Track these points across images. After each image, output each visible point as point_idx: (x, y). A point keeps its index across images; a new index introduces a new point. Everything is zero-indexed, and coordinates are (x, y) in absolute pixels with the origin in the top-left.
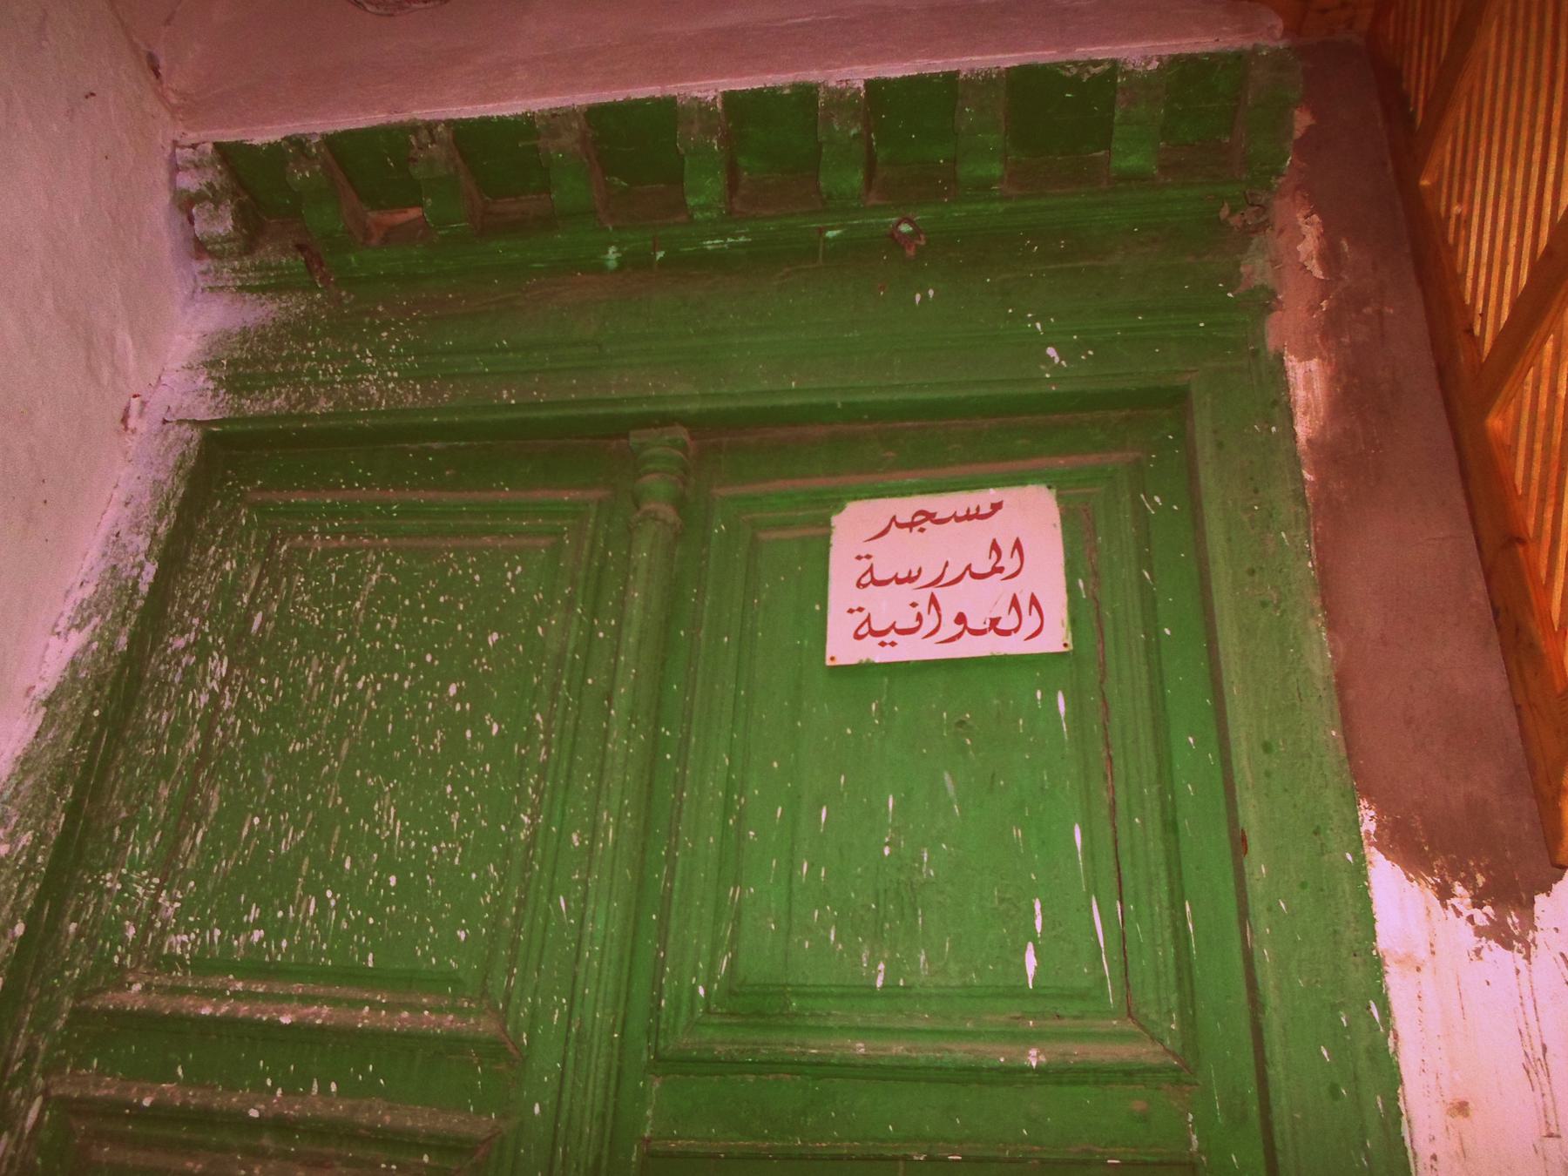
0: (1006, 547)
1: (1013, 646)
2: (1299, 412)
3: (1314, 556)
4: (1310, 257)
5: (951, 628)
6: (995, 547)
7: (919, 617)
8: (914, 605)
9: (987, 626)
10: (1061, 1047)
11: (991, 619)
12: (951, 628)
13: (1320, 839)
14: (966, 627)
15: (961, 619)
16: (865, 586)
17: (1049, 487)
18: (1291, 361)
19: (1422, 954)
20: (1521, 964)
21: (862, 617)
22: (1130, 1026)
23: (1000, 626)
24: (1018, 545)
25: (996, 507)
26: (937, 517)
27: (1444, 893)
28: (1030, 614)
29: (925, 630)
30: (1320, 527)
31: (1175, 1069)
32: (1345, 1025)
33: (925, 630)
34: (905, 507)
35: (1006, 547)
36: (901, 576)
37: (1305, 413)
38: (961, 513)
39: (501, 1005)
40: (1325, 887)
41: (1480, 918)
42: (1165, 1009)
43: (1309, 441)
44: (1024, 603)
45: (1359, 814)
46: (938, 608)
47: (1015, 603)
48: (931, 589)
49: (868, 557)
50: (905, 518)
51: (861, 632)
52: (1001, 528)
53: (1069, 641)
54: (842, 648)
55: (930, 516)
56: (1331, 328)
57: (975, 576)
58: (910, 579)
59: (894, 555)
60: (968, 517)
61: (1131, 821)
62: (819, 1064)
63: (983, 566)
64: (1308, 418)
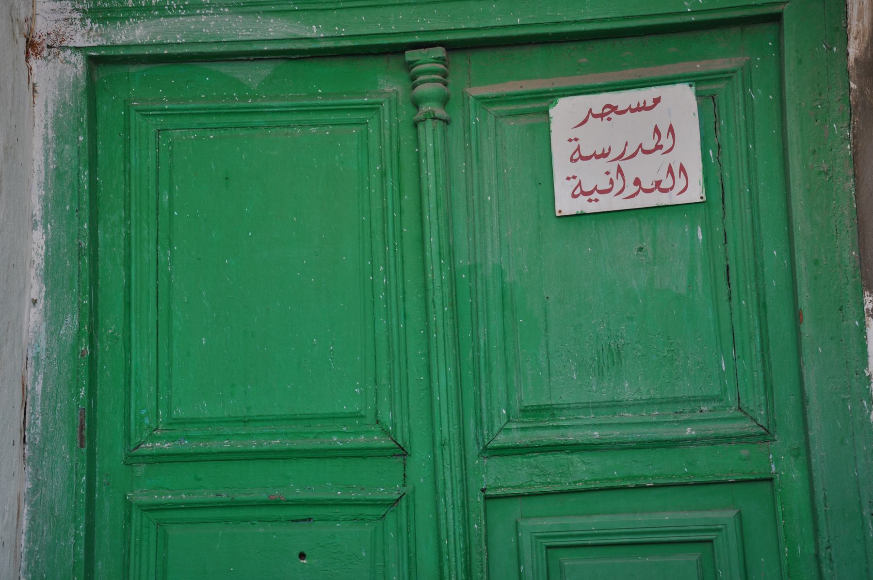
0: (664, 131)
1: (672, 198)
3: (852, 142)
5: (631, 189)
6: (657, 131)
7: (611, 182)
8: (607, 173)
9: (654, 186)
10: (703, 426)
11: (656, 181)
12: (631, 189)
13: (842, 313)
14: (641, 187)
15: (637, 182)
16: (576, 160)
17: (691, 86)
21: (576, 182)
22: (739, 414)
23: (662, 186)
24: (671, 129)
25: (657, 101)
26: (619, 109)
28: (680, 177)
29: (616, 189)
30: (857, 122)
31: (762, 434)
32: (850, 409)
33: (616, 189)
34: (597, 101)
36: (598, 153)
37: (856, 38)
38: (634, 106)
39: (390, 428)
40: (843, 339)
42: (758, 404)
43: (856, 60)
45: (864, 299)
46: (623, 175)
47: (670, 170)
48: (618, 162)
49: (576, 139)
51: (576, 193)
52: (658, 117)
53: (704, 195)
55: (614, 109)
58: (604, 155)
60: (639, 109)
61: (740, 302)
62: (575, 444)
63: (650, 145)
64: (857, 41)
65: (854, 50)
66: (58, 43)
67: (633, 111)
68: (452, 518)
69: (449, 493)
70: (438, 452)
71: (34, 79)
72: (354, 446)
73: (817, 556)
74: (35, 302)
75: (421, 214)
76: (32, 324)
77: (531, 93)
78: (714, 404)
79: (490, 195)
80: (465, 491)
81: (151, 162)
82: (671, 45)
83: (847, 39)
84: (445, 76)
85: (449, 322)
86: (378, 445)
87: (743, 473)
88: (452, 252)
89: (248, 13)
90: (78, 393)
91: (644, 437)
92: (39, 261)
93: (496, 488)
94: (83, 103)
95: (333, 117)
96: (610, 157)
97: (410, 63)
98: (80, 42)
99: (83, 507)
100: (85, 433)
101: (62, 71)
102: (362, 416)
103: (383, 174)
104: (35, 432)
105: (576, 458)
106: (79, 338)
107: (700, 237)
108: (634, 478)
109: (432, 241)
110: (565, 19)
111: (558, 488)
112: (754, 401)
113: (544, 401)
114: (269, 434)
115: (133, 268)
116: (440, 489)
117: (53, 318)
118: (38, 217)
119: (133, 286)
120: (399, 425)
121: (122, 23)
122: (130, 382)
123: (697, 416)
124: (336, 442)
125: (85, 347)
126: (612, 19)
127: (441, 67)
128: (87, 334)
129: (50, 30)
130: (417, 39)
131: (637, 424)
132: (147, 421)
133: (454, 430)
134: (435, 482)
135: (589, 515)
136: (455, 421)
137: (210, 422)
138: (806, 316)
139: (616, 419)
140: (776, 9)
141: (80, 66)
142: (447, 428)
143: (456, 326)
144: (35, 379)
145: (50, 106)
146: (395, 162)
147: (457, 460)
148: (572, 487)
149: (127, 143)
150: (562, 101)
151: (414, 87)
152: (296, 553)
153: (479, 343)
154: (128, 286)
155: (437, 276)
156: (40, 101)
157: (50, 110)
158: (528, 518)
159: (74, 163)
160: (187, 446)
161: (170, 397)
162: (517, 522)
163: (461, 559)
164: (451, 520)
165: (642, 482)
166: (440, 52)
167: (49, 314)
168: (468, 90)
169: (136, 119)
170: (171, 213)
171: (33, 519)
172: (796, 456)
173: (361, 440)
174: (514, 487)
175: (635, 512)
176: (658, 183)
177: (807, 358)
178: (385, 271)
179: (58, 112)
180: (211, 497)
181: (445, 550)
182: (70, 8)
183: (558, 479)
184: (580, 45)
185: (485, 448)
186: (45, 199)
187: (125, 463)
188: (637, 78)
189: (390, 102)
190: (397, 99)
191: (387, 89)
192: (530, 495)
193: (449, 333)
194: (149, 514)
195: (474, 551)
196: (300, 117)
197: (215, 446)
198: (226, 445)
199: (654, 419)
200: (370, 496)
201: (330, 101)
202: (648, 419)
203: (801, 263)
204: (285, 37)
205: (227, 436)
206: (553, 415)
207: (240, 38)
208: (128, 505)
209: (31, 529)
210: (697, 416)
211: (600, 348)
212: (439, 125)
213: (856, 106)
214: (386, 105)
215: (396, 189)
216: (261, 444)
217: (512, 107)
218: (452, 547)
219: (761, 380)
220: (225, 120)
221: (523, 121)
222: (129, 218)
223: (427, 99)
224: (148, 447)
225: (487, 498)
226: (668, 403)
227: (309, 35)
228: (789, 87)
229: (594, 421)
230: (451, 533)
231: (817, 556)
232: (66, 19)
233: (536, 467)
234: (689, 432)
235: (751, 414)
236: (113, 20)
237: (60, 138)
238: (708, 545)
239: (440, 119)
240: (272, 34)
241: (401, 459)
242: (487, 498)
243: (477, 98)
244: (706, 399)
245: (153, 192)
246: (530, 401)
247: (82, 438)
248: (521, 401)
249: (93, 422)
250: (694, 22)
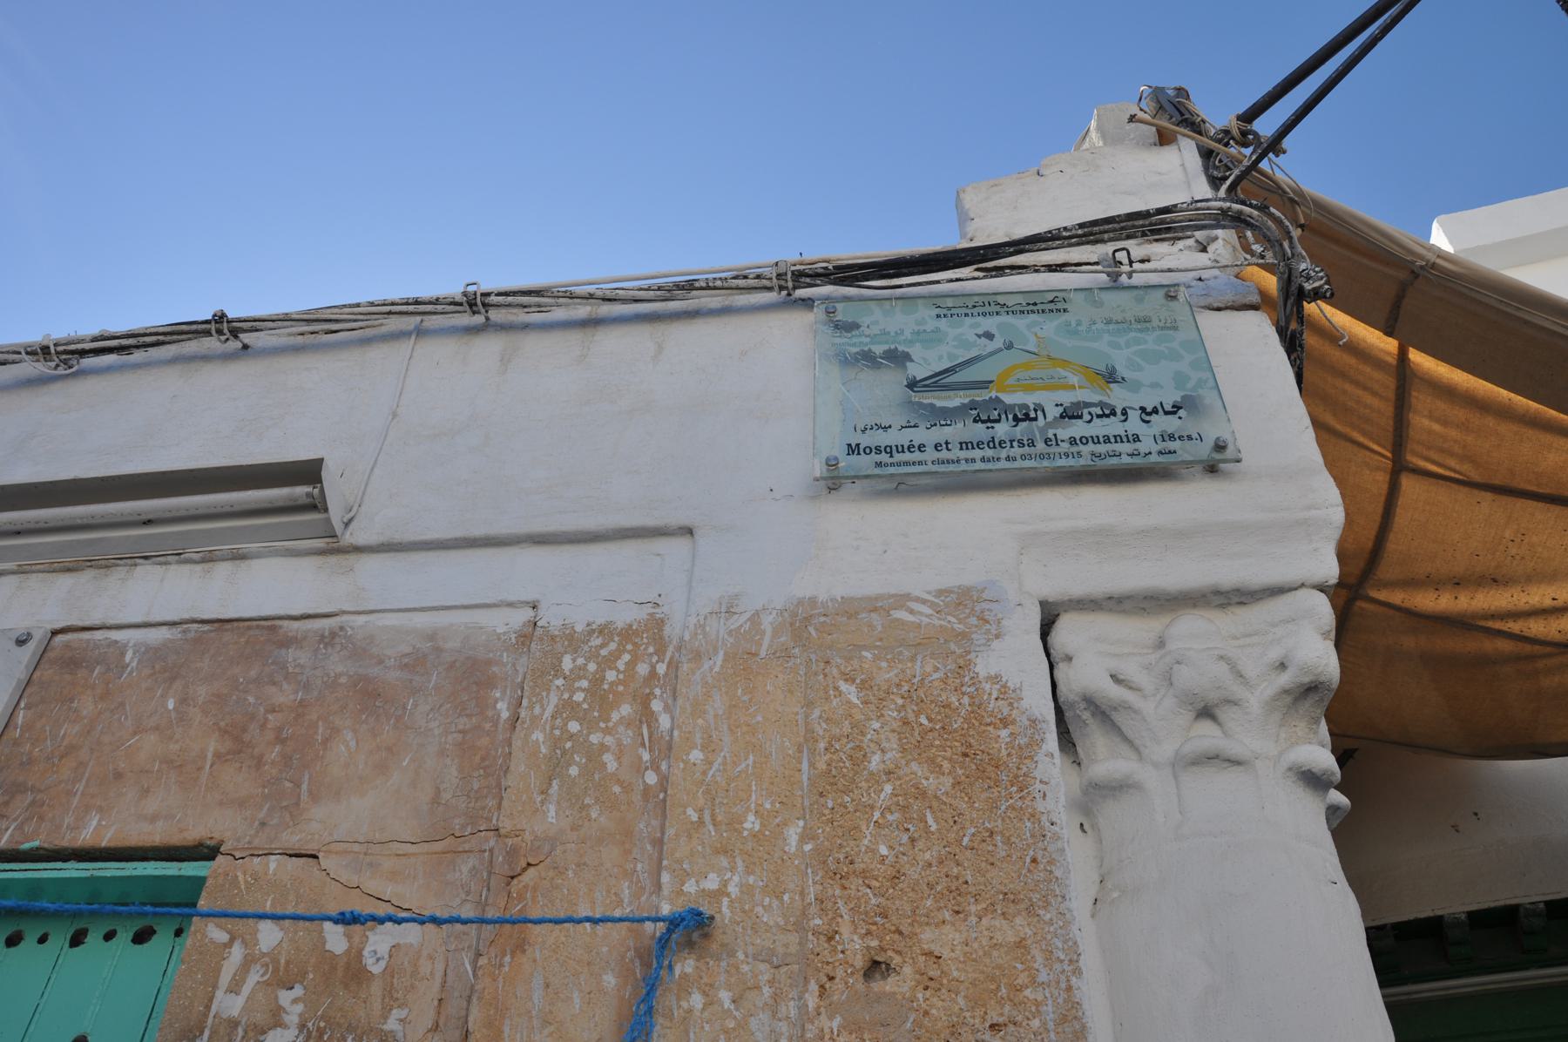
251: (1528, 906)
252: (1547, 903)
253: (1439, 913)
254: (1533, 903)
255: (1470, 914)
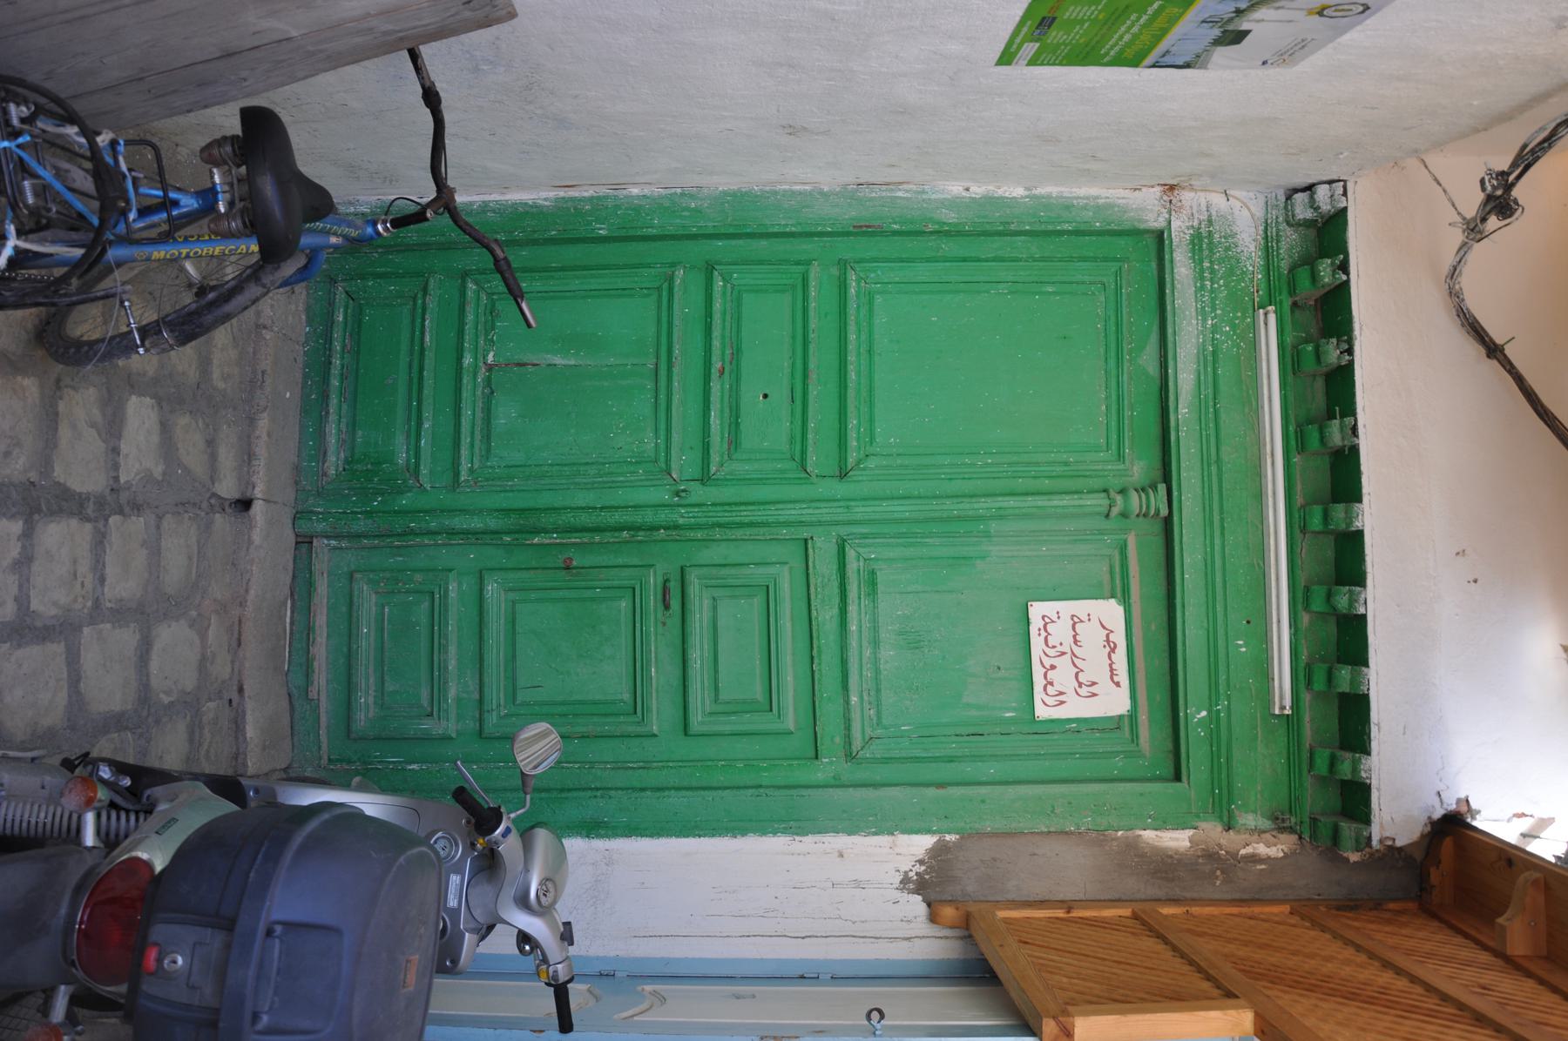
1: (1038, 689)
2: (1158, 833)
4: (1254, 848)
6: (1094, 684)
7: (1054, 647)
8: (1061, 644)
10: (858, 710)
15: (1053, 667)
18: (1190, 832)
19: (897, 850)
20: (895, 886)
21: (1055, 618)
22: (867, 738)
23: (1049, 687)
24: (1094, 695)
25: (1118, 684)
27: (921, 862)
29: (1049, 651)
33: (1049, 651)
34: (1119, 638)
35: (1093, 689)
41: (911, 874)
44: (1061, 698)
47: (1061, 693)
50: (1112, 637)
52: (1105, 684)
54: (1037, 610)
55: (1113, 650)
56: (1211, 856)
57: (1077, 674)
58: (1076, 642)
59: (1091, 636)
60: (1112, 670)
63: (1082, 678)
65: (1149, 835)
66: (1173, 208)
67: (1111, 665)
68: (791, 513)
69: (810, 511)
70: (841, 504)
71: (1144, 189)
72: (849, 438)
73: (760, 786)
74: (967, 190)
75: (1033, 494)
76: (950, 188)
77: (1128, 584)
78: (875, 719)
79: (1047, 550)
80: (811, 524)
81: (1079, 278)
82: (1162, 696)
83: (1156, 830)
84: (1145, 515)
85: (945, 515)
86: (849, 456)
87: (822, 738)
88: (1001, 517)
89: (1198, 358)
90: (895, 223)
91: (850, 665)
92: (1000, 192)
93: (813, 548)
94: (1127, 226)
95: (1114, 424)
96: (1074, 647)
97: (1156, 488)
98: (1174, 225)
99: (808, 229)
100: (864, 229)
101: (1152, 211)
102: (871, 443)
103: (1066, 464)
104: (865, 192)
105: (836, 611)
106: (938, 223)
107: (1007, 715)
108: (820, 656)
109: (1011, 502)
110: (1187, 613)
111: (812, 597)
112: (876, 750)
113: (880, 588)
114: (860, 372)
115: (994, 264)
116: (813, 505)
117: (954, 203)
118: (1034, 192)
119: (978, 264)
120: (864, 473)
121: (1190, 258)
122: (903, 262)
123: (866, 706)
124: (853, 422)
125: (931, 227)
126: (1185, 651)
127: (1152, 512)
128: (941, 229)
129: (1183, 202)
130: (1175, 494)
131: (861, 660)
132: (872, 275)
133: (859, 517)
134: (818, 501)
135: (792, 619)
136: (866, 517)
137: (870, 325)
138: (941, 792)
139: (865, 643)
140: (1184, 778)
141: (1155, 224)
142: (860, 511)
143: (942, 520)
144: (907, 191)
145: (1124, 201)
146: (1075, 473)
147: (836, 519)
148: (813, 608)
149: (1095, 259)
150: (1121, 609)
151: (1136, 490)
152: (767, 392)
153: (927, 537)
154: (979, 260)
155: (982, 506)
156: (1127, 193)
157: (1120, 201)
158: (790, 573)
159: (1078, 219)
160: (852, 306)
161: (891, 293)
162: (787, 563)
163: (759, 519)
164: (788, 512)
165: (816, 661)
166: (1164, 512)
167: (958, 200)
168: (1133, 533)
169: (1114, 266)
170: (1037, 293)
171: (800, 193)
172: (834, 777)
173: (853, 443)
174: (814, 562)
175: (793, 654)
176: (1051, 684)
177: (908, 790)
178: (987, 464)
179: (1119, 207)
180: (812, 325)
181: (767, 507)
182: (1202, 218)
183: (819, 596)
184: (1165, 625)
185: (844, 541)
186: (1049, 196)
187: (840, 259)
188: (1136, 670)
189: (1125, 470)
190: (1127, 476)
191: (1135, 468)
192: (808, 575)
193: (937, 514)
194: (800, 279)
195: (765, 529)
196: (1114, 397)
197: (852, 328)
198: (852, 337)
199: (864, 673)
200: (810, 449)
201: (1126, 422)
202: (864, 669)
203: (983, 790)
204: (1179, 387)
205: (858, 337)
206: (869, 595)
207: (1178, 350)
208: (808, 263)
209: (793, 192)
210: (866, 706)
211: (921, 633)
212: (1104, 510)
213: (1104, 835)
214: (1122, 467)
215: (1054, 474)
216: (852, 364)
217: (1117, 569)
218: (770, 513)
219: (893, 756)
220: (1112, 338)
221: (1107, 577)
222: (1035, 261)
223: (1126, 501)
224: (852, 277)
225: (806, 540)
226: (877, 684)
227: (1180, 406)
228: (1122, 787)
229: (864, 627)
230: (780, 512)
231: (760, 786)
232: (1192, 215)
233: (829, 580)
234: (854, 699)
235: (867, 746)
236: (1193, 251)
237: (1098, 208)
238: (768, 708)
239: (1109, 511)
240: (1181, 376)
241: (838, 473)
242: (806, 540)
243: (1125, 541)
244: (879, 714)
245: (1055, 279)
246: (880, 577)
247: (861, 227)
248: (881, 569)
249: (873, 234)
250: (1178, 715)
251: (1363, 596)
252: (1364, 617)
253: (1365, 499)
254: (1366, 603)
255: (1359, 534)
